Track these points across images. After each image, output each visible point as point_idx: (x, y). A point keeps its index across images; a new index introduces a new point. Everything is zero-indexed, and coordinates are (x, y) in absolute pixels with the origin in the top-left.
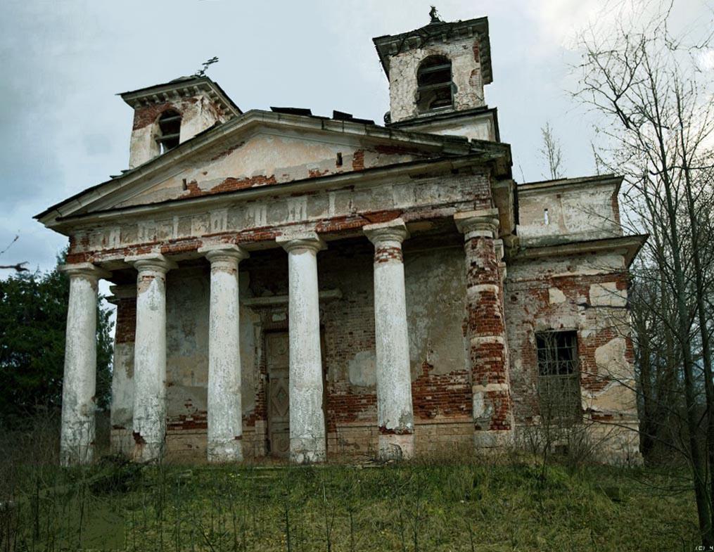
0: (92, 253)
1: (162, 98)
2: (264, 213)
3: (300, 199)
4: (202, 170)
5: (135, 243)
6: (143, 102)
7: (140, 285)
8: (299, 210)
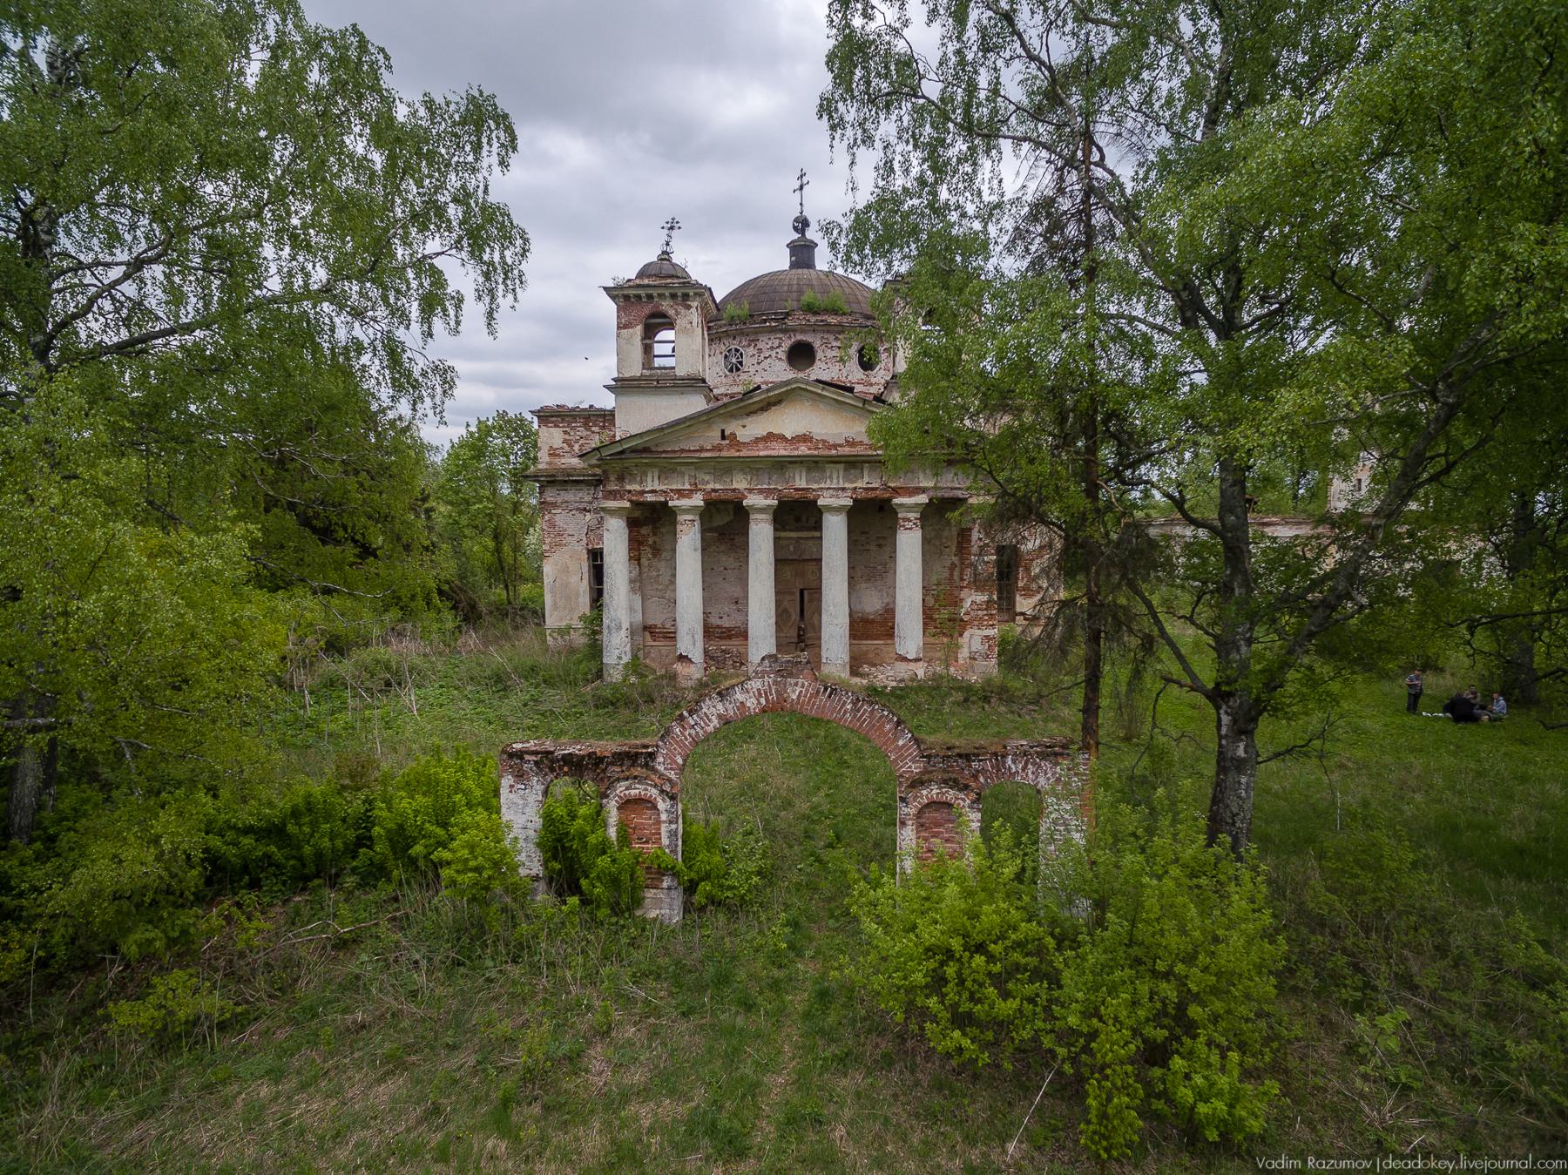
0: (630, 492)
1: (650, 297)
2: (804, 474)
3: (838, 466)
4: (740, 422)
5: (674, 487)
6: (627, 297)
7: (679, 528)
8: (836, 478)
